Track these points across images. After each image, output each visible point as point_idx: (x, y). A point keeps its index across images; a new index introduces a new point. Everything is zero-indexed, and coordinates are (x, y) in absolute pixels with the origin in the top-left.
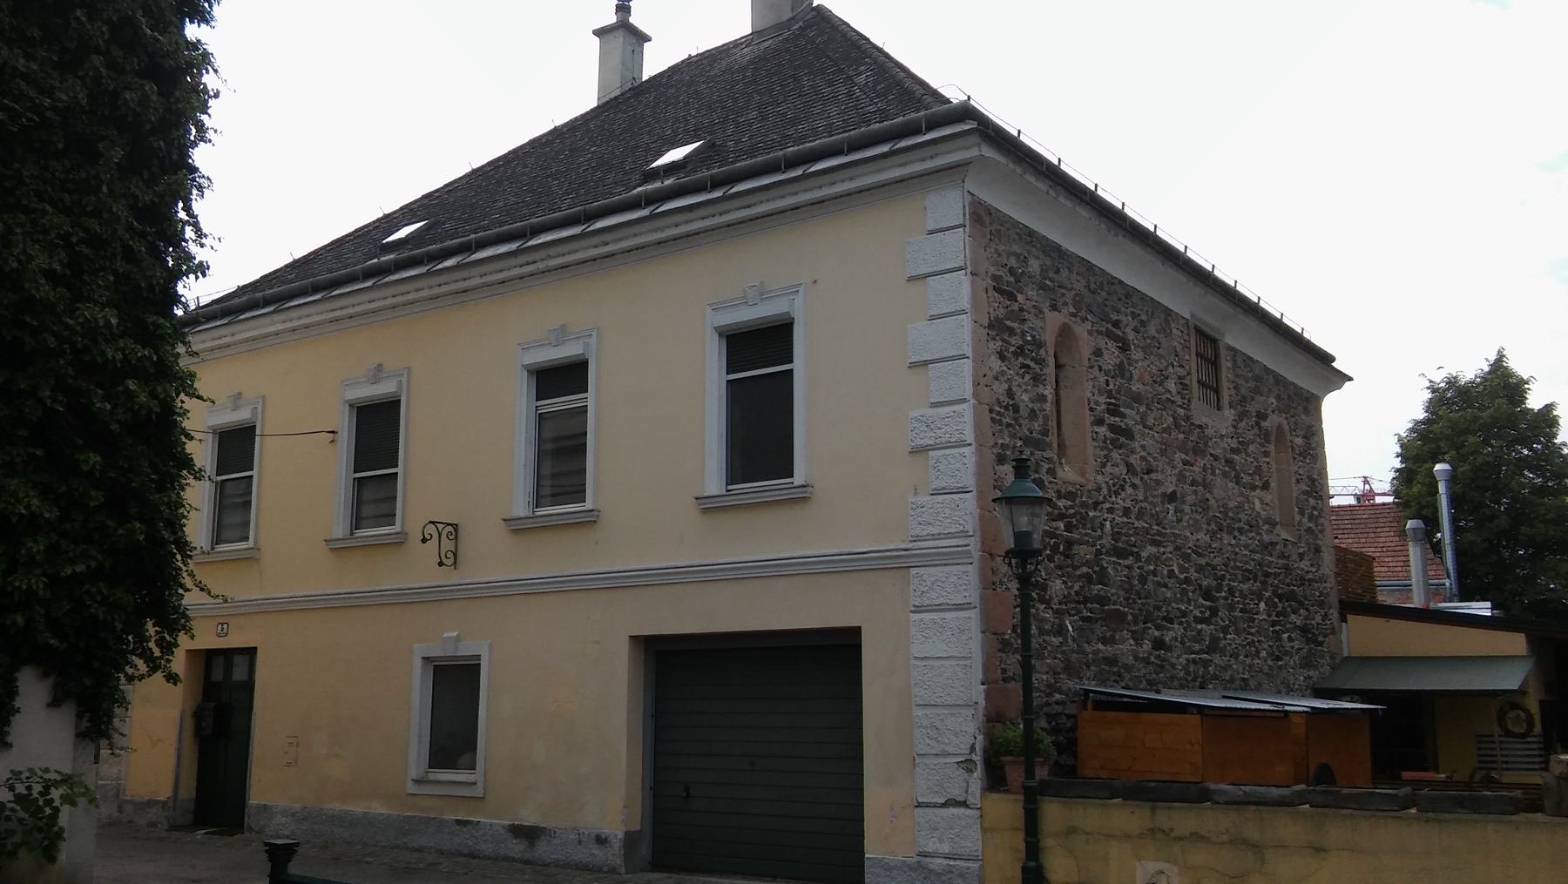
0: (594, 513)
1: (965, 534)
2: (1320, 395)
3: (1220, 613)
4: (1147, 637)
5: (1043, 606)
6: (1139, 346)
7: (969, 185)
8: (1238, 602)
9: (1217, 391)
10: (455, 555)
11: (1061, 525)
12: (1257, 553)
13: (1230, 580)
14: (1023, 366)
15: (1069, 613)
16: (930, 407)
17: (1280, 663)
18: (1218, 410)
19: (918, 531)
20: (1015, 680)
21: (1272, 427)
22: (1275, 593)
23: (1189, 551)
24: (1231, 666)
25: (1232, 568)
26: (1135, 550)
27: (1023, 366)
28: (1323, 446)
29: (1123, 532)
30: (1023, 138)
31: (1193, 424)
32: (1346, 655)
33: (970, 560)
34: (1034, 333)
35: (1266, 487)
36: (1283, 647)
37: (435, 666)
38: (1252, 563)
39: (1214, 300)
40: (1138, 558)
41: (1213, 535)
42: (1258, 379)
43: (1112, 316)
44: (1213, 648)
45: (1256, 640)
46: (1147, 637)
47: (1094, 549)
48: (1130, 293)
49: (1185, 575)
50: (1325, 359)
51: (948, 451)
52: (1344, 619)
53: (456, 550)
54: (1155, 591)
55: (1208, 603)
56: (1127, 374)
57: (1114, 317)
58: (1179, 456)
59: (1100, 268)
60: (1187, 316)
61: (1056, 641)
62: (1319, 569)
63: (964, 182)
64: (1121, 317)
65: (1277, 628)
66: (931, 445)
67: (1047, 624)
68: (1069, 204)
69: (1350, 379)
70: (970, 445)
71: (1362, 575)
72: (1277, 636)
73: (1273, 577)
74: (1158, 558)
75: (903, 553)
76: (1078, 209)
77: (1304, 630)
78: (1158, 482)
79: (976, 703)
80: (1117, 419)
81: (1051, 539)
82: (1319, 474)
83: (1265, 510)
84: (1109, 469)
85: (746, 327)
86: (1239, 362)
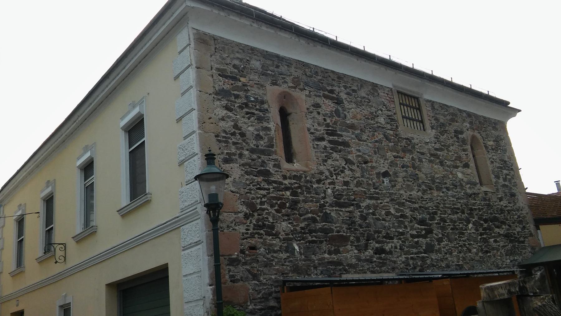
0: (93, 228)
1: (196, 203)
2: (504, 121)
3: (434, 232)
4: (370, 248)
5: (271, 237)
6: (351, 102)
7: (191, 25)
8: (449, 225)
9: (422, 122)
10: (65, 258)
11: (288, 193)
12: (463, 199)
13: (441, 214)
14: (247, 113)
15: (295, 240)
16: (184, 140)
17: (489, 254)
18: (424, 131)
19: (182, 206)
20: (242, 280)
21: (467, 137)
22: (480, 218)
23: (404, 201)
24: (447, 258)
25: (442, 208)
26: (355, 202)
27: (247, 113)
28: (510, 144)
29: (344, 194)
30: (315, 31)
31: (401, 138)
32: (542, 246)
33: (199, 216)
34: (256, 96)
35: (466, 166)
36: (490, 245)
37: (64, 309)
38: (459, 205)
39: (407, 77)
40: (358, 206)
41: (424, 192)
42: (453, 114)
43: (327, 88)
44: (430, 249)
45: (467, 243)
46: (370, 248)
47: (318, 204)
48: (340, 77)
49: (401, 213)
50: (504, 104)
51: (189, 161)
52: (538, 228)
53: (65, 256)
54: (374, 223)
55: (423, 227)
56: (342, 115)
57: (329, 88)
58: (389, 154)
59: (314, 65)
60: (391, 87)
61: (284, 255)
62: (515, 204)
63: (188, 24)
64: (334, 88)
65: (485, 236)
66: (184, 159)
67: (276, 247)
68: (272, 31)
69: (520, 111)
70: (197, 154)
71: (554, 206)
72: (485, 241)
73: (478, 211)
74: (377, 206)
75: (177, 219)
76: (279, 33)
77: (507, 236)
78: (373, 168)
79: (204, 297)
80: (336, 137)
81: (278, 201)
82: (509, 158)
83: (466, 178)
84: (330, 162)
85: (131, 124)
86: (436, 107)
